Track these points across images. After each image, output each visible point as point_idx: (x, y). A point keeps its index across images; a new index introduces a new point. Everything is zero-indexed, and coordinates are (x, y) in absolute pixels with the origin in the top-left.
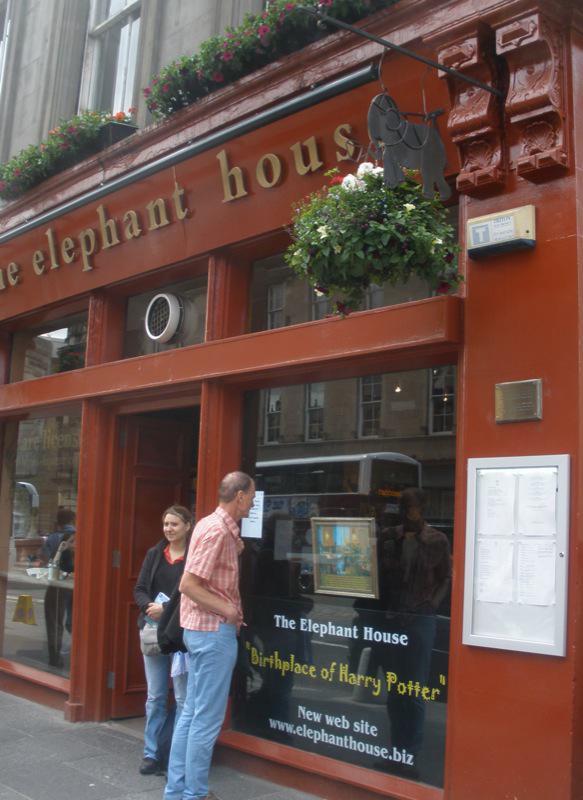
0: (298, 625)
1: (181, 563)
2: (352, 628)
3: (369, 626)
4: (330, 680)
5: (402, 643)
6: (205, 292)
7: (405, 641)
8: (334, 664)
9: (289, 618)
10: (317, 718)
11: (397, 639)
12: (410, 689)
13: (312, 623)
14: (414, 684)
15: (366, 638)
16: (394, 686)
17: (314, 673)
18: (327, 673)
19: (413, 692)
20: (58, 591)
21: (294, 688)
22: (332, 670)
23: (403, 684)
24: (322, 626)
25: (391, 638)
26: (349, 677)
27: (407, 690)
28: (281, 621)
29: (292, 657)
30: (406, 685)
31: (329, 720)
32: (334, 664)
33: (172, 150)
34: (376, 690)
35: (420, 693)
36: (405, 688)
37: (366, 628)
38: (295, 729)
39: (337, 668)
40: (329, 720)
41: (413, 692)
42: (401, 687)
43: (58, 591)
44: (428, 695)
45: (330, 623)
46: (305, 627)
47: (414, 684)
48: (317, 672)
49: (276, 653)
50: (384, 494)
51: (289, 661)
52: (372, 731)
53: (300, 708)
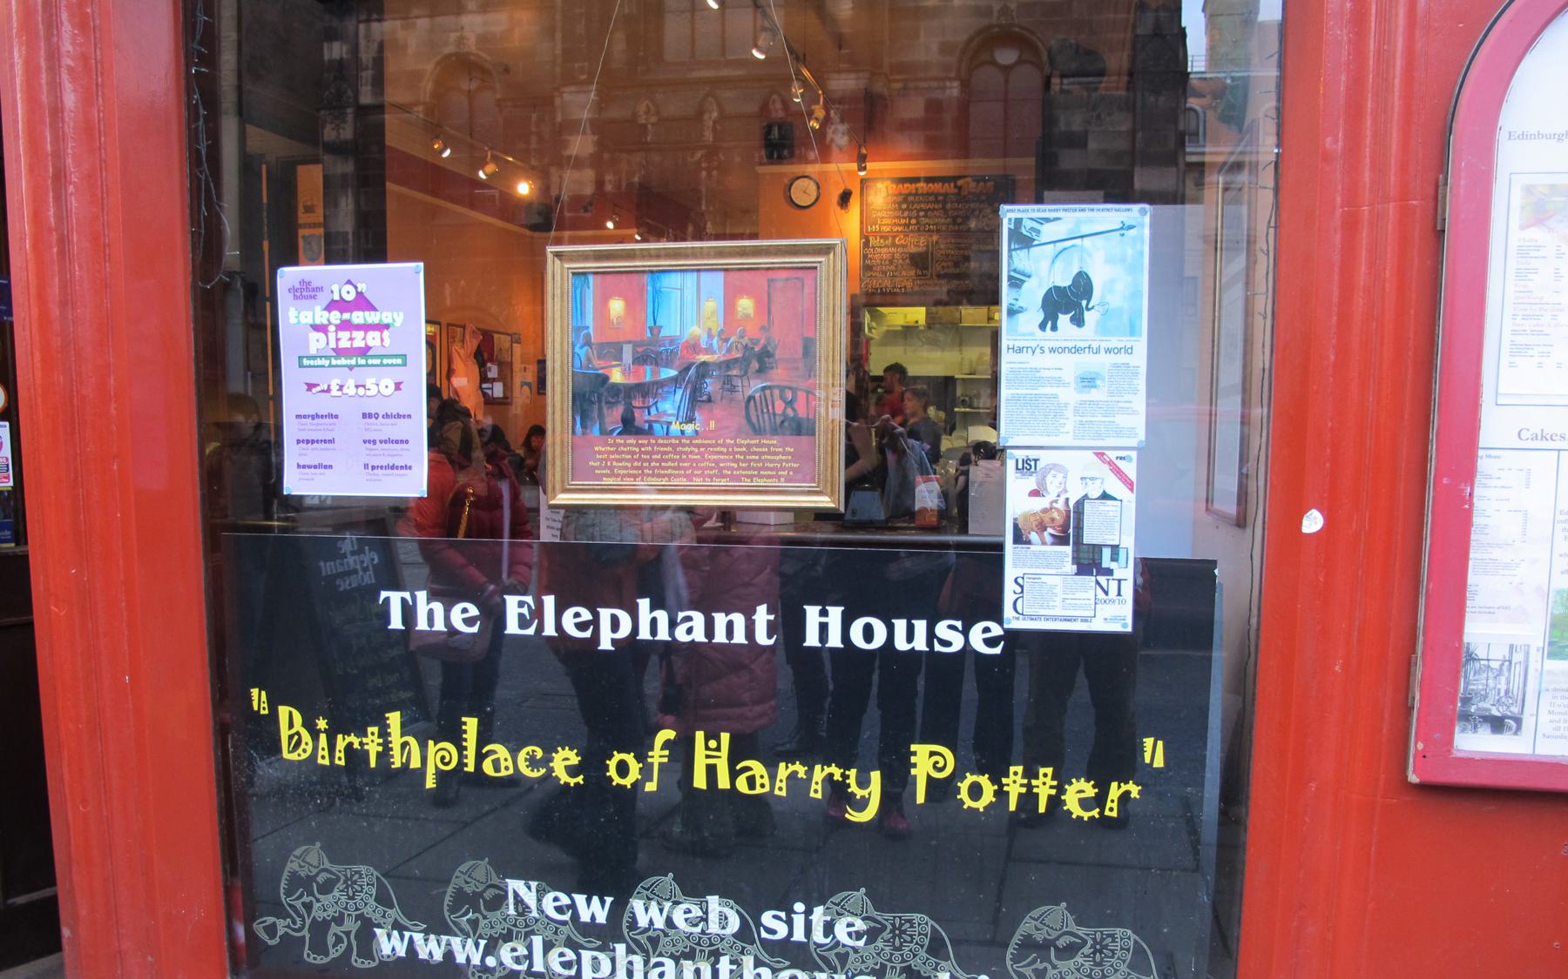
0: (493, 616)
3: (824, 602)
4: (651, 787)
6: (837, 532)
7: (990, 642)
9: (448, 593)
10: (595, 910)
14: (1031, 774)
16: (941, 789)
20: (47, 892)
22: (658, 756)
24: (605, 614)
25: (931, 635)
26: (734, 775)
27: (1001, 794)
28: (409, 612)
30: (995, 780)
33: (779, 251)
34: (862, 805)
37: (812, 612)
39: (682, 751)
41: (1029, 798)
43: (47, 892)
46: (523, 623)
47: (1031, 774)
49: (394, 719)
51: (457, 739)
52: (841, 932)
53: (255, 692)
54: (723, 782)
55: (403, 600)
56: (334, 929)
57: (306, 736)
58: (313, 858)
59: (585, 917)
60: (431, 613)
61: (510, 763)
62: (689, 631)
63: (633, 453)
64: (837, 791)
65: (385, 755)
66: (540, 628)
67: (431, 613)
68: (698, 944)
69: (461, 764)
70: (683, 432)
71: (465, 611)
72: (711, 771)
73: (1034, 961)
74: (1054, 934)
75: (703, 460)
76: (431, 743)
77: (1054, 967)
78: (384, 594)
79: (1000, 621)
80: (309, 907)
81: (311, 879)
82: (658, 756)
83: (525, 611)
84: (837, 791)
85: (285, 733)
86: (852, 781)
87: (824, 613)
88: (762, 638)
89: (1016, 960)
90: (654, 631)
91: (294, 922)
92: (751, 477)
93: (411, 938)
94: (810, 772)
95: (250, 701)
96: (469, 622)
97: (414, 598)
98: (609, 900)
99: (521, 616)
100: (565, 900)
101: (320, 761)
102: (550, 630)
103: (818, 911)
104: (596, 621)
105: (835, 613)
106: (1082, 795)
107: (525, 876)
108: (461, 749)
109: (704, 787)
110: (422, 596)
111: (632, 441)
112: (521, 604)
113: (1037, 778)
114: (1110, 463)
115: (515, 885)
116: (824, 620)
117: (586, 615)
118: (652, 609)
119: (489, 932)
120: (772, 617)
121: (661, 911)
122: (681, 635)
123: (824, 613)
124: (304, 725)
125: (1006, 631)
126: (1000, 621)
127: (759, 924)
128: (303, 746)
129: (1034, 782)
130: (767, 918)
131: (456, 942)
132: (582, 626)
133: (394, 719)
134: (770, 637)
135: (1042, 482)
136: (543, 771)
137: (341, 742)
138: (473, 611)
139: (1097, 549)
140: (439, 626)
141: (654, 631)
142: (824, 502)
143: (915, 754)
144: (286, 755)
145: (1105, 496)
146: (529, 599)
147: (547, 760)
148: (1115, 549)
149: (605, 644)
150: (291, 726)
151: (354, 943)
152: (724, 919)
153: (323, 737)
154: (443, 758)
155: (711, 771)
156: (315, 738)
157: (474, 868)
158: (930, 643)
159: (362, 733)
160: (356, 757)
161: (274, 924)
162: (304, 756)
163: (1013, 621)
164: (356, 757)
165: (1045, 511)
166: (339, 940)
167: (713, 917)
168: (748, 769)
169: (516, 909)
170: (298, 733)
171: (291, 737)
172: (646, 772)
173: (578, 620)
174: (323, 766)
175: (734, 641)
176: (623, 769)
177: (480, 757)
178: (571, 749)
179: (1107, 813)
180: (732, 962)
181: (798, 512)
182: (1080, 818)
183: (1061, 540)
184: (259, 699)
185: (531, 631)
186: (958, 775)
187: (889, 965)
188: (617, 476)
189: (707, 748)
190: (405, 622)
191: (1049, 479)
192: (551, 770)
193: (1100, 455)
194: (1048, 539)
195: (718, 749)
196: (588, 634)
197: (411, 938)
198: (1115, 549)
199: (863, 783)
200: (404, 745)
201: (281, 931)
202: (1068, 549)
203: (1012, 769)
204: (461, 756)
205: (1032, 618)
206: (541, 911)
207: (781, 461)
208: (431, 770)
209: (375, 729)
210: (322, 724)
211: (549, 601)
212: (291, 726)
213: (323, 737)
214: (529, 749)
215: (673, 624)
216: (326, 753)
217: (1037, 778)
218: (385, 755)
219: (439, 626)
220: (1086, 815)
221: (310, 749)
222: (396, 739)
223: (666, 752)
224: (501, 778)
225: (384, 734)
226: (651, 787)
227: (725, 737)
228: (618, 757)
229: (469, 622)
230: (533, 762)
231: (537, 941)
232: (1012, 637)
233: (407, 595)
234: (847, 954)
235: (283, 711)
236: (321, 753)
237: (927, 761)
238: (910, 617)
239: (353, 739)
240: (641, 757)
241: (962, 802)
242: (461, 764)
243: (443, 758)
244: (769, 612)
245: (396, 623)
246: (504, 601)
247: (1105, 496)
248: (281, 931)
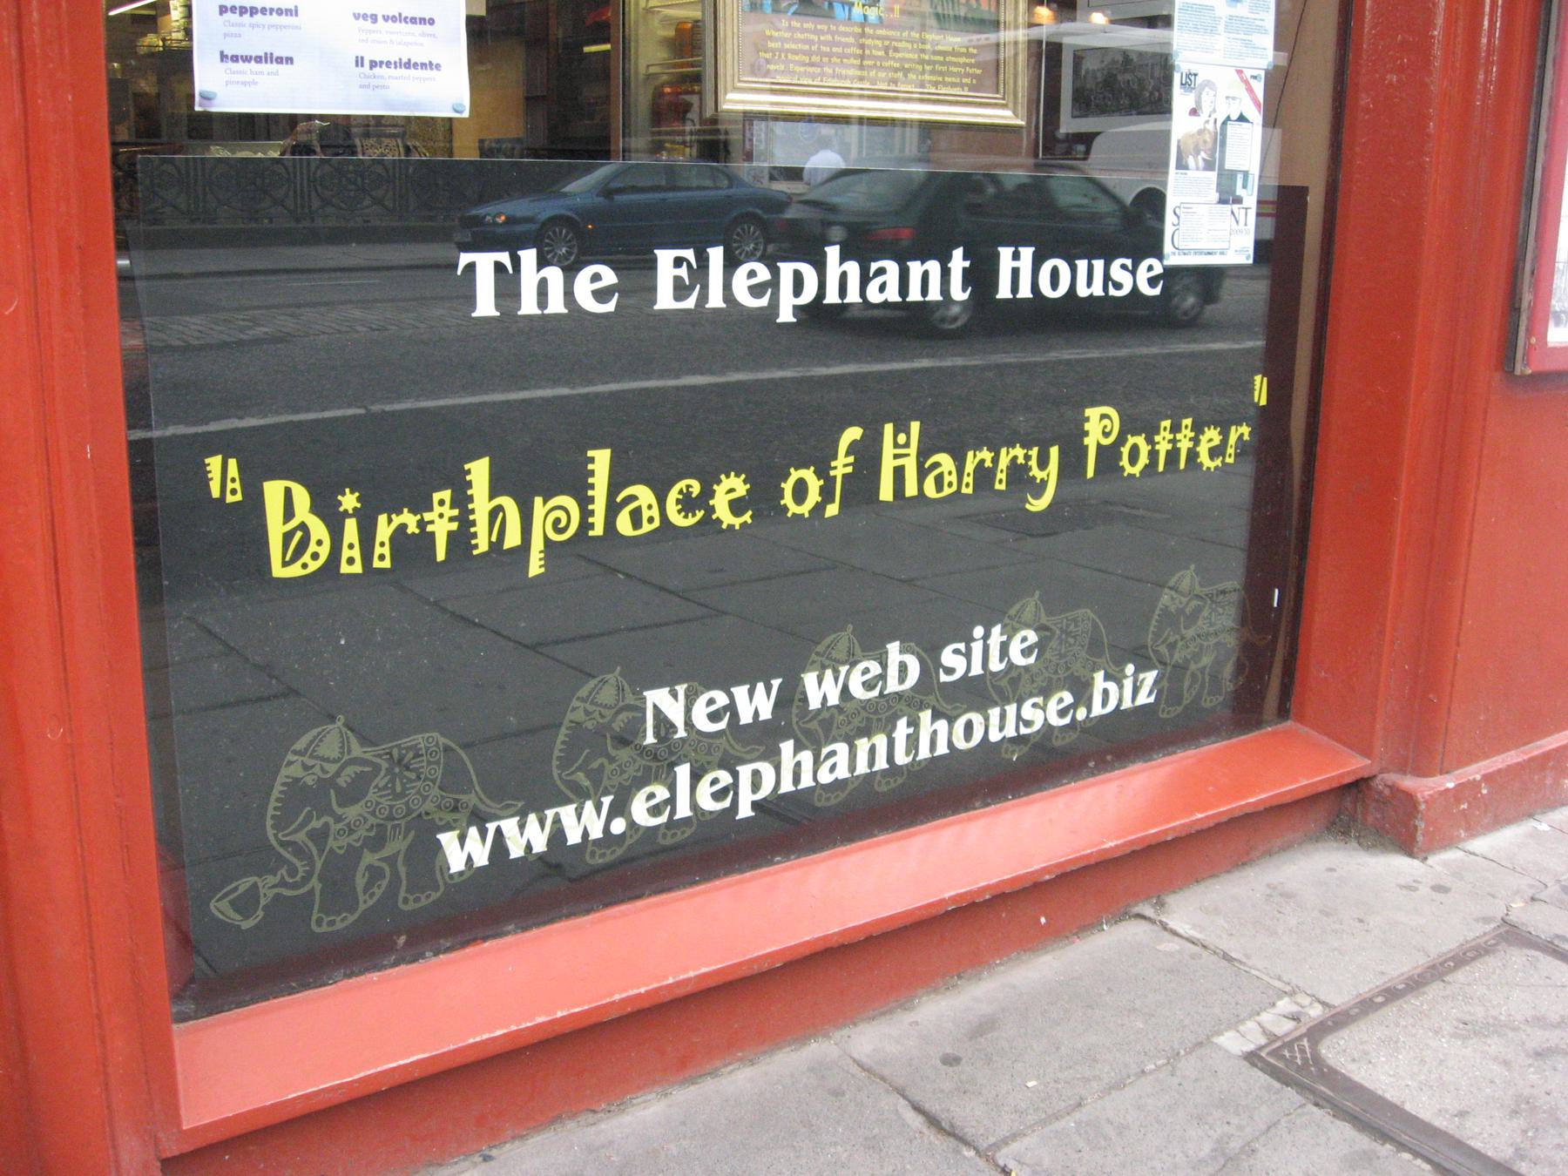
1: (109, 60)
2: (945, 261)
3: (1016, 242)
5: (1146, 290)
8: (853, 433)
10: (755, 703)
11: (1125, 279)
12: (1184, 445)
13: (731, 264)
15: (1004, 292)
16: (1108, 455)
17: (737, 507)
18: (814, 484)
19: (1173, 455)
21: (1260, 343)
23: (1140, 440)
24: (787, 269)
25: (1107, 277)
26: (922, 474)
28: (507, 283)
29: (601, 461)
30: (1150, 441)
31: (820, 690)
32: (853, 433)
35: (1193, 455)
36: (1144, 449)
37: (1005, 253)
38: (558, 835)
39: (867, 456)
40: (820, 690)
42: (1135, 451)
44: (1215, 452)
45: (833, 252)
46: (681, 290)
48: (762, 499)
49: (479, 472)
50: (1451, 785)
53: (1258, 378)
54: (911, 490)
55: (499, 267)
56: (369, 858)
57: (318, 529)
58: (330, 748)
59: (746, 718)
60: (543, 287)
61: (655, 512)
62: (882, 288)
63: (811, 42)
64: (1018, 472)
65: (461, 538)
66: (703, 297)
67: (543, 287)
68: (876, 712)
69: (585, 525)
70: (865, 17)
71: (596, 277)
72: (899, 473)
73: (588, 760)
74: (332, 768)
75: (887, 57)
76: (538, 501)
77: (612, 759)
78: (465, 258)
79: (1160, 257)
80: (320, 837)
81: (326, 784)
82: (841, 466)
83: (683, 272)
84: (1018, 472)
85: (276, 528)
86: (1033, 463)
87: (1016, 256)
88: (959, 294)
89: (562, 767)
90: (843, 291)
91: (293, 871)
92: (936, 84)
93: (499, 831)
94: (995, 460)
95: (206, 482)
96: (601, 295)
97: (516, 262)
98: (776, 683)
99: (678, 281)
100: (721, 699)
101: (345, 569)
102: (716, 300)
103: (996, 630)
104: (774, 283)
105: (1027, 253)
106: (733, 496)
107: (669, 682)
108: (585, 502)
109: (890, 498)
110: (529, 257)
111: (809, 25)
112: (678, 262)
113: (431, 509)
114: (1246, 82)
115: (658, 697)
116: (1016, 264)
117: (763, 274)
118: (843, 260)
119: (616, 780)
120: (967, 264)
121: (836, 680)
122: (874, 296)
123: (1016, 256)
124: (315, 509)
125: (1166, 268)
126: (1160, 257)
127: (938, 664)
128: (312, 547)
129: (427, 516)
130: (948, 657)
131: (567, 813)
132: (756, 291)
133: (479, 472)
134: (964, 290)
135: (1198, 101)
136: (700, 514)
137: (384, 529)
138: (609, 277)
139: (1232, 174)
140: (556, 305)
141: (843, 291)
142: (1003, 116)
143: (592, 460)
144: (278, 571)
145: (1242, 119)
146: (689, 254)
147: (707, 493)
148: (1246, 174)
149: (786, 315)
150: (289, 513)
151: (403, 871)
152: (903, 668)
153: (351, 526)
154: (557, 521)
155: (899, 473)
156: (335, 525)
157: (318, 739)
158: (1105, 288)
159: (422, 504)
160: (411, 547)
161: (255, 885)
162: (314, 566)
163: (1173, 259)
164: (411, 547)
165: (1200, 132)
166: (375, 874)
167: (893, 671)
168: (633, 498)
169: (656, 734)
170: (303, 527)
171: (288, 537)
172: (827, 493)
173: (754, 281)
174: (352, 577)
175: (1019, 296)
176: (800, 492)
177: (613, 510)
178: (719, 482)
179: (377, 564)
180: (909, 725)
181: (929, 128)
182: (731, 527)
183: (1209, 166)
184: (222, 476)
185: (690, 303)
186: (1121, 440)
187: (389, 825)
188: (793, 73)
189: (896, 445)
190: (942, 293)
191: (1204, 96)
192: (712, 510)
193: (1240, 72)
194: (1201, 164)
195: (907, 445)
196: (763, 302)
197: (499, 831)
198: (1246, 174)
199: (1043, 463)
200: (495, 512)
201: (266, 895)
202: (1213, 175)
203: (437, 496)
204: (586, 513)
205: (1185, 253)
206: (689, 724)
207: (965, 65)
208: (537, 544)
209: (446, 495)
210: (349, 501)
211: (716, 255)
212: (289, 513)
213: (351, 526)
214: (682, 484)
215: (865, 280)
216: (356, 553)
217: (431, 509)
218: (461, 538)
219: (556, 305)
220: (737, 522)
221: (324, 552)
222: (481, 505)
223: (851, 459)
224: (314, 573)
225: (462, 500)
226: (832, 510)
227: (915, 426)
228: (795, 475)
229: (601, 295)
230: (687, 504)
231: (683, 772)
232: (1171, 273)
233: (504, 257)
234: (832, 717)
235: (273, 491)
236: (346, 553)
237: (1099, 424)
238: (1090, 257)
239: (409, 520)
240: (823, 472)
241: (786, 509)
242: (585, 525)
243: (557, 521)
244: (965, 258)
245: (486, 306)
246: (998, 255)
247: (1242, 119)
248: (266, 895)
